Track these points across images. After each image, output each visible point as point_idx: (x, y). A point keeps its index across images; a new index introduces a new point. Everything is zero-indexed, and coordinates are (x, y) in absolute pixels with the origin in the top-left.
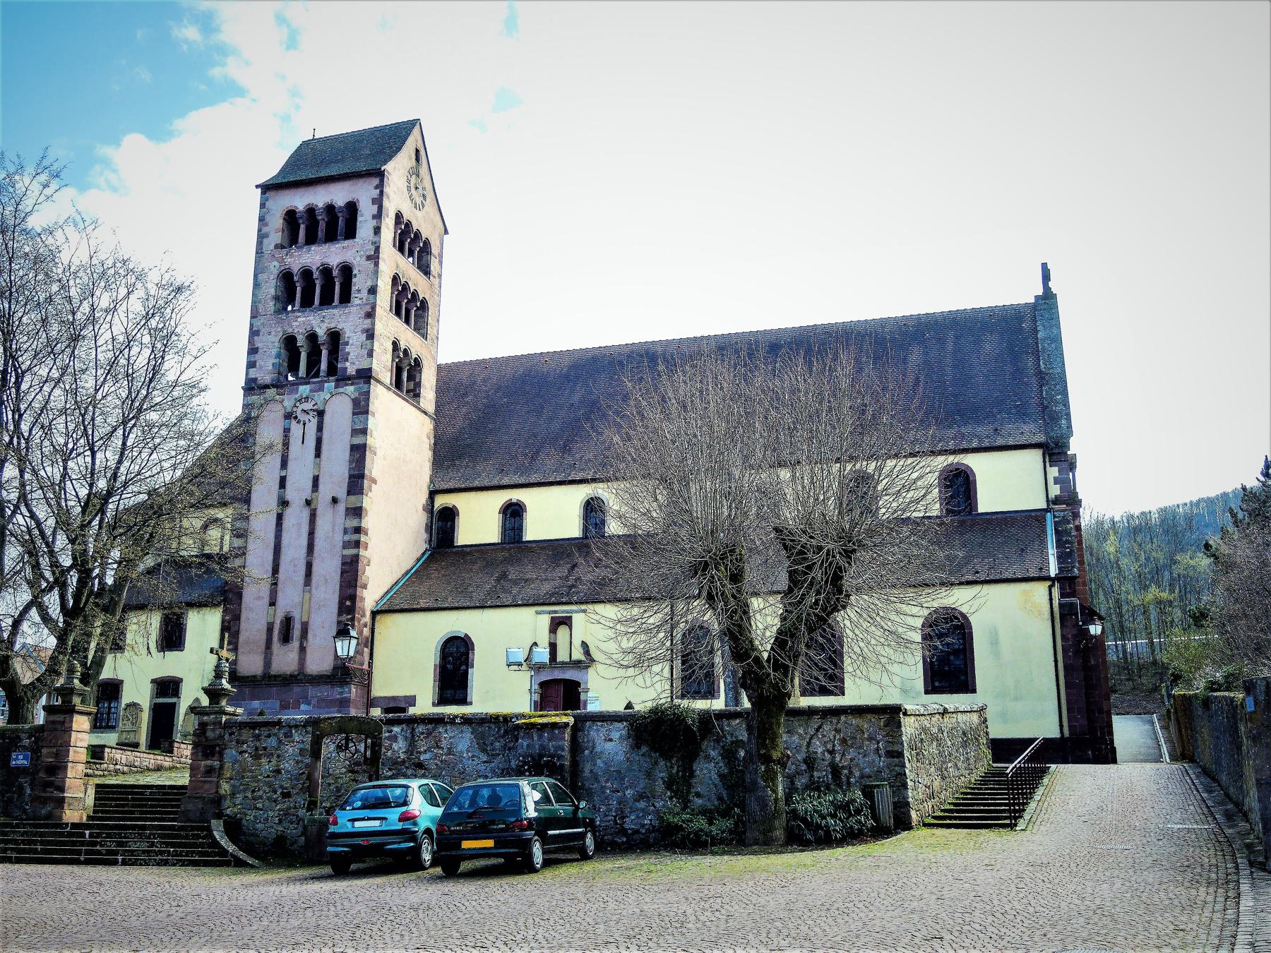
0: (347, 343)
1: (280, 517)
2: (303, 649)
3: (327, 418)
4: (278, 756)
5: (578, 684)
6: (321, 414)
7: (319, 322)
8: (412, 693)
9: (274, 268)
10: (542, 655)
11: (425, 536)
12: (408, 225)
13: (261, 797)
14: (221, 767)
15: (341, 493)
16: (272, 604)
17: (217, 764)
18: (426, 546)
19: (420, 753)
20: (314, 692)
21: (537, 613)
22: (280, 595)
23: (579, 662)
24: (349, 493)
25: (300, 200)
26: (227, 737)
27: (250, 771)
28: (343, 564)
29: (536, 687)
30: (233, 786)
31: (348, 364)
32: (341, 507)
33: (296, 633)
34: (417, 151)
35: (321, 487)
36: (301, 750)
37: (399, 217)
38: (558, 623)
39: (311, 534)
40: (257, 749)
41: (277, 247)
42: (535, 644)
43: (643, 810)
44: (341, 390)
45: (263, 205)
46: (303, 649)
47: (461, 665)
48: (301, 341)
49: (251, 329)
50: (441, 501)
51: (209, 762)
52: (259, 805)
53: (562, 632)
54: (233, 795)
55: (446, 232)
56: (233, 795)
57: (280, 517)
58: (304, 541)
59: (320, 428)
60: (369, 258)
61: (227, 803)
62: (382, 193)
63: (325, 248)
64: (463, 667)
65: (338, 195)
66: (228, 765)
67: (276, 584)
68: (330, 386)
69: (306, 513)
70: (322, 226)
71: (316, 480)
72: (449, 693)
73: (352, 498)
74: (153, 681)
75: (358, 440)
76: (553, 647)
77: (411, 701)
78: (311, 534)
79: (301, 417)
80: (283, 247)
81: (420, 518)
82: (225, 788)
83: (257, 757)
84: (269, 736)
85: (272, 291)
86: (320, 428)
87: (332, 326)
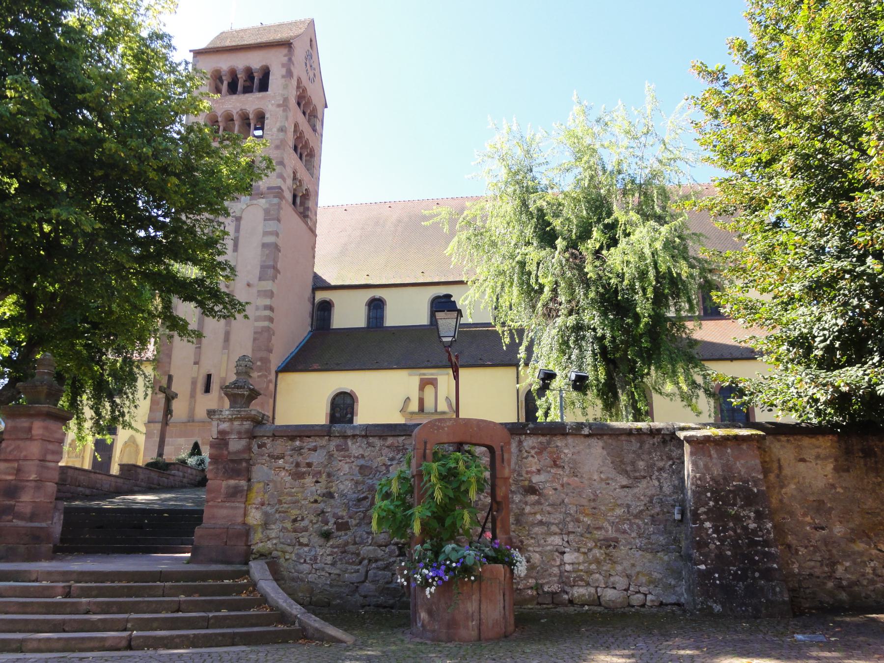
3: (242, 222)
4: (329, 475)
10: (414, 407)
11: (309, 320)
12: (305, 90)
13: (305, 529)
14: (249, 489)
15: (254, 280)
17: (243, 483)
18: (310, 329)
19: (531, 472)
21: (410, 375)
24: (260, 279)
25: (225, 64)
26: (255, 448)
27: (290, 494)
28: (255, 333)
30: (266, 514)
32: (254, 290)
34: (311, 41)
36: (361, 467)
37: (299, 81)
38: (424, 384)
40: (298, 465)
42: (408, 398)
43: (861, 554)
44: (255, 202)
47: (347, 414)
50: (320, 296)
51: (232, 482)
52: (304, 540)
53: (429, 390)
54: (266, 525)
55: (326, 107)
56: (266, 525)
60: (279, 106)
61: (257, 536)
62: (290, 60)
64: (349, 416)
65: (255, 61)
66: (257, 487)
67: (200, 348)
70: (241, 84)
73: (263, 283)
75: (271, 239)
76: (421, 401)
81: (308, 307)
82: (255, 517)
83: (298, 475)
84: (315, 449)
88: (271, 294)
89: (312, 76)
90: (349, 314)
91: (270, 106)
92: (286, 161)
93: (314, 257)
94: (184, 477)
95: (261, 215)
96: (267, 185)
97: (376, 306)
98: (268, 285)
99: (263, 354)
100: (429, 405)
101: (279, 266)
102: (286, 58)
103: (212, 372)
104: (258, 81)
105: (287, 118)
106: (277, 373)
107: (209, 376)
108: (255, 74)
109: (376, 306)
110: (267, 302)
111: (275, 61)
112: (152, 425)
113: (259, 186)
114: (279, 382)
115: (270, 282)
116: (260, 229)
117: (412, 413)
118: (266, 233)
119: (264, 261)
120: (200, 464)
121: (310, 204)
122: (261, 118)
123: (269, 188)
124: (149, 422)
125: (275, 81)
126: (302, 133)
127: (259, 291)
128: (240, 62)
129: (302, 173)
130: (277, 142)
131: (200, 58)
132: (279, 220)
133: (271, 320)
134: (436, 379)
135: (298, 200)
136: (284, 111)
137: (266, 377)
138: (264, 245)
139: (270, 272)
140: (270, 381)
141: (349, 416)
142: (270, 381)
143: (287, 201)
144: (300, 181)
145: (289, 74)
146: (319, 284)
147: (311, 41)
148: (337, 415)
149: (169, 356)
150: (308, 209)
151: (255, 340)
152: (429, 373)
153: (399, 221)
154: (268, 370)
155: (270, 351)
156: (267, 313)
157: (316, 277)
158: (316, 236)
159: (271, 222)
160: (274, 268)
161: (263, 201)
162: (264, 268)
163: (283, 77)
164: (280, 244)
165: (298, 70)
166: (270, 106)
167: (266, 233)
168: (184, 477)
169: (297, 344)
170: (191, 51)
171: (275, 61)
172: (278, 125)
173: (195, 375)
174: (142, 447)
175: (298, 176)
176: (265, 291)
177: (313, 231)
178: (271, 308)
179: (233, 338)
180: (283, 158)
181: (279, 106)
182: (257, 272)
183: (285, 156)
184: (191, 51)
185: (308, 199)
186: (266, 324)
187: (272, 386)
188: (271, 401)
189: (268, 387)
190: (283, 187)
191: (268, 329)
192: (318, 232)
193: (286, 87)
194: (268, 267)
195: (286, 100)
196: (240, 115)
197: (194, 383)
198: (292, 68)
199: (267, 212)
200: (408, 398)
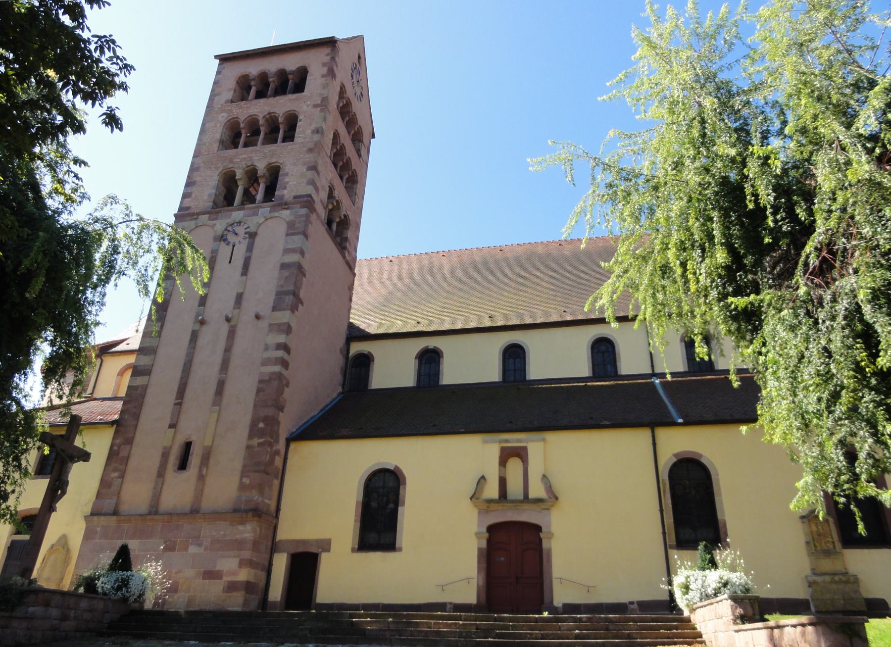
0: (287, 174)
1: (194, 336)
2: (201, 478)
3: (258, 240)
5: (538, 529)
6: (252, 236)
7: (260, 157)
8: (328, 537)
9: (223, 117)
10: (492, 491)
11: (340, 378)
16: (173, 426)
18: (340, 389)
20: (209, 531)
21: (485, 442)
22: (183, 417)
23: (539, 501)
24: (274, 309)
25: (253, 68)
28: (260, 382)
29: (485, 530)
31: (285, 192)
32: (264, 324)
33: (195, 460)
34: (359, 57)
35: (245, 304)
38: (506, 455)
39: (228, 350)
41: (227, 102)
42: (483, 478)
44: (276, 214)
45: (218, 73)
46: (201, 478)
47: (388, 502)
48: (239, 174)
49: (191, 166)
50: (357, 348)
53: (514, 465)
55: (373, 137)
57: (194, 336)
58: (218, 358)
59: (250, 248)
62: (333, 59)
63: (271, 100)
64: (391, 506)
65: (291, 63)
67: (180, 404)
68: (265, 210)
69: (225, 328)
71: (239, 298)
72: (372, 537)
73: (278, 314)
74: (400, 550)
75: (294, 258)
76: (503, 482)
77: (326, 545)
78: (228, 350)
79: (231, 238)
80: (232, 102)
81: (336, 363)
85: (218, 136)
86: (250, 248)
87: (273, 160)
88: (287, 329)
89: (358, 94)
90: (394, 370)
91: (305, 108)
92: (320, 168)
93: (351, 300)
94: (64, 618)
95: (282, 228)
96: (293, 194)
97: (430, 360)
98: (284, 316)
99: (269, 412)
100: (515, 489)
101: (302, 294)
102: (329, 57)
103: (193, 438)
104: (295, 82)
105: (325, 119)
106: (289, 441)
107: (188, 445)
108: (290, 77)
109: (430, 360)
110: (282, 339)
111: (315, 62)
112: (95, 518)
113: (283, 196)
114: (290, 455)
115: (287, 313)
116: (281, 246)
117: (490, 501)
118: (287, 251)
119: (282, 286)
120: (119, 588)
121: (349, 234)
122: (292, 122)
123: (295, 197)
124: (92, 514)
125: (313, 83)
126: (343, 147)
127: (271, 325)
128: (272, 65)
129: (340, 192)
130: (311, 145)
131: (227, 65)
132: (306, 236)
133: (285, 364)
134: (525, 449)
135: (334, 226)
136: (322, 111)
137: (271, 445)
138: (284, 266)
139: (289, 299)
140: (277, 453)
141: (391, 506)
142: (277, 453)
143: (318, 215)
144: (337, 202)
145: (331, 73)
146: (356, 334)
147: (359, 57)
148: (374, 504)
149: (137, 417)
150: (346, 239)
151: (259, 391)
152: (515, 439)
153: (456, 268)
154: (275, 436)
155: (281, 409)
156: (280, 353)
157: (351, 326)
158: (354, 275)
159: (294, 237)
160: (295, 294)
161: (287, 212)
162: (280, 294)
163: (323, 76)
164: (306, 266)
165: (343, 75)
166: (305, 108)
167: (287, 251)
168: (64, 618)
169: (321, 407)
170: (216, 57)
171: (315, 62)
172: (313, 126)
173: (167, 443)
174: (75, 553)
175: (336, 194)
176: (279, 325)
177: (350, 266)
178: (285, 348)
179: (228, 389)
180: (316, 162)
181: (315, 106)
182: (271, 301)
183: (320, 162)
184: (216, 57)
185: (347, 229)
186: (277, 368)
187: (278, 461)
188: (276, 483)
189: (272, 461)
190: (315, 197)
191: (279, 376)
192: (356, 271)
193: (325, 86)
194: (287, 293)
195: (325, 100)
196: (267, 120)
197: (165, 455)
198: (335, 68)
199: (291, 225)
200: (483, 478)
